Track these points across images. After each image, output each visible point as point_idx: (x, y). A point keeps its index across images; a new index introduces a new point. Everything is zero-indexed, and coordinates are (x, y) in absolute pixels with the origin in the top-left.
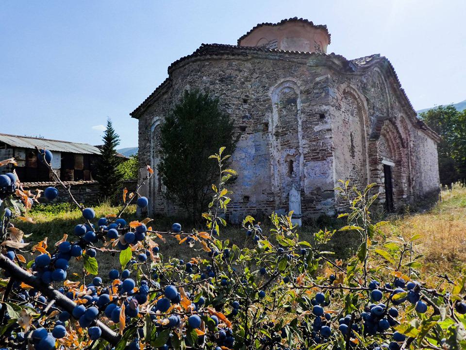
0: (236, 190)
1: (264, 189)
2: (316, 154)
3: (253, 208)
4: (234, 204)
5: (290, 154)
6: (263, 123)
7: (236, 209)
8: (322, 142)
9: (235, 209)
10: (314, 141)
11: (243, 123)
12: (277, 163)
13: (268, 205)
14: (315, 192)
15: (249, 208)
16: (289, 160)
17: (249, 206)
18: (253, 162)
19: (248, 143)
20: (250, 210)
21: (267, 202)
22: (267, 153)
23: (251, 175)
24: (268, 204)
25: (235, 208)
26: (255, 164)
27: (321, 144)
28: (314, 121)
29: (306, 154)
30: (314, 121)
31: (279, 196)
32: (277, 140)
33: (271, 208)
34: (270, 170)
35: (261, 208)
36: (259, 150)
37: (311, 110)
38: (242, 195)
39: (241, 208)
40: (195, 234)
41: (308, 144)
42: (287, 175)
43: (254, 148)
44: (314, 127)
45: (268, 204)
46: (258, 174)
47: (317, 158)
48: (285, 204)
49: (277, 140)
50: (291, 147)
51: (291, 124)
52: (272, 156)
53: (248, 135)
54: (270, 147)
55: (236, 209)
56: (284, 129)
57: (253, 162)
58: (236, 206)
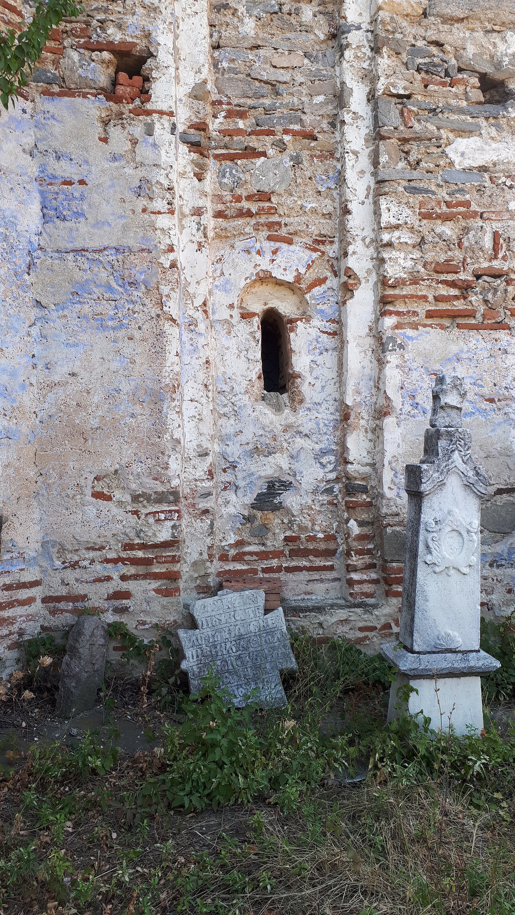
2: (454, 292)
3: (24, 594)
5: (277, 274)
6: (110, 47)
8: (489, 228)
10: (446, 218)
13: (132, 570)
16: (258, 308)
20: (10, 605)
23: (13, 375)
24: (135, 562)
27: (488, 242)
28: (452, 110)
29: (399, 283)
30: (452, 110)
31: (206, 512)
32: (200, 178)
33: (155, 584)
35: (81, 589)
36: (79, 214)
37: (439, 44)
40: (306, 663)
41: (412, 229)
44: (449, 143)
45: (135, 562)
47: (453, 315)
48: (239, 558)
49: (200, 178)
50: (283, 232)
51: (287, 99)
52: (173, 265)
54: (160, 204)
56: (241, 124)
57: (25, 287)
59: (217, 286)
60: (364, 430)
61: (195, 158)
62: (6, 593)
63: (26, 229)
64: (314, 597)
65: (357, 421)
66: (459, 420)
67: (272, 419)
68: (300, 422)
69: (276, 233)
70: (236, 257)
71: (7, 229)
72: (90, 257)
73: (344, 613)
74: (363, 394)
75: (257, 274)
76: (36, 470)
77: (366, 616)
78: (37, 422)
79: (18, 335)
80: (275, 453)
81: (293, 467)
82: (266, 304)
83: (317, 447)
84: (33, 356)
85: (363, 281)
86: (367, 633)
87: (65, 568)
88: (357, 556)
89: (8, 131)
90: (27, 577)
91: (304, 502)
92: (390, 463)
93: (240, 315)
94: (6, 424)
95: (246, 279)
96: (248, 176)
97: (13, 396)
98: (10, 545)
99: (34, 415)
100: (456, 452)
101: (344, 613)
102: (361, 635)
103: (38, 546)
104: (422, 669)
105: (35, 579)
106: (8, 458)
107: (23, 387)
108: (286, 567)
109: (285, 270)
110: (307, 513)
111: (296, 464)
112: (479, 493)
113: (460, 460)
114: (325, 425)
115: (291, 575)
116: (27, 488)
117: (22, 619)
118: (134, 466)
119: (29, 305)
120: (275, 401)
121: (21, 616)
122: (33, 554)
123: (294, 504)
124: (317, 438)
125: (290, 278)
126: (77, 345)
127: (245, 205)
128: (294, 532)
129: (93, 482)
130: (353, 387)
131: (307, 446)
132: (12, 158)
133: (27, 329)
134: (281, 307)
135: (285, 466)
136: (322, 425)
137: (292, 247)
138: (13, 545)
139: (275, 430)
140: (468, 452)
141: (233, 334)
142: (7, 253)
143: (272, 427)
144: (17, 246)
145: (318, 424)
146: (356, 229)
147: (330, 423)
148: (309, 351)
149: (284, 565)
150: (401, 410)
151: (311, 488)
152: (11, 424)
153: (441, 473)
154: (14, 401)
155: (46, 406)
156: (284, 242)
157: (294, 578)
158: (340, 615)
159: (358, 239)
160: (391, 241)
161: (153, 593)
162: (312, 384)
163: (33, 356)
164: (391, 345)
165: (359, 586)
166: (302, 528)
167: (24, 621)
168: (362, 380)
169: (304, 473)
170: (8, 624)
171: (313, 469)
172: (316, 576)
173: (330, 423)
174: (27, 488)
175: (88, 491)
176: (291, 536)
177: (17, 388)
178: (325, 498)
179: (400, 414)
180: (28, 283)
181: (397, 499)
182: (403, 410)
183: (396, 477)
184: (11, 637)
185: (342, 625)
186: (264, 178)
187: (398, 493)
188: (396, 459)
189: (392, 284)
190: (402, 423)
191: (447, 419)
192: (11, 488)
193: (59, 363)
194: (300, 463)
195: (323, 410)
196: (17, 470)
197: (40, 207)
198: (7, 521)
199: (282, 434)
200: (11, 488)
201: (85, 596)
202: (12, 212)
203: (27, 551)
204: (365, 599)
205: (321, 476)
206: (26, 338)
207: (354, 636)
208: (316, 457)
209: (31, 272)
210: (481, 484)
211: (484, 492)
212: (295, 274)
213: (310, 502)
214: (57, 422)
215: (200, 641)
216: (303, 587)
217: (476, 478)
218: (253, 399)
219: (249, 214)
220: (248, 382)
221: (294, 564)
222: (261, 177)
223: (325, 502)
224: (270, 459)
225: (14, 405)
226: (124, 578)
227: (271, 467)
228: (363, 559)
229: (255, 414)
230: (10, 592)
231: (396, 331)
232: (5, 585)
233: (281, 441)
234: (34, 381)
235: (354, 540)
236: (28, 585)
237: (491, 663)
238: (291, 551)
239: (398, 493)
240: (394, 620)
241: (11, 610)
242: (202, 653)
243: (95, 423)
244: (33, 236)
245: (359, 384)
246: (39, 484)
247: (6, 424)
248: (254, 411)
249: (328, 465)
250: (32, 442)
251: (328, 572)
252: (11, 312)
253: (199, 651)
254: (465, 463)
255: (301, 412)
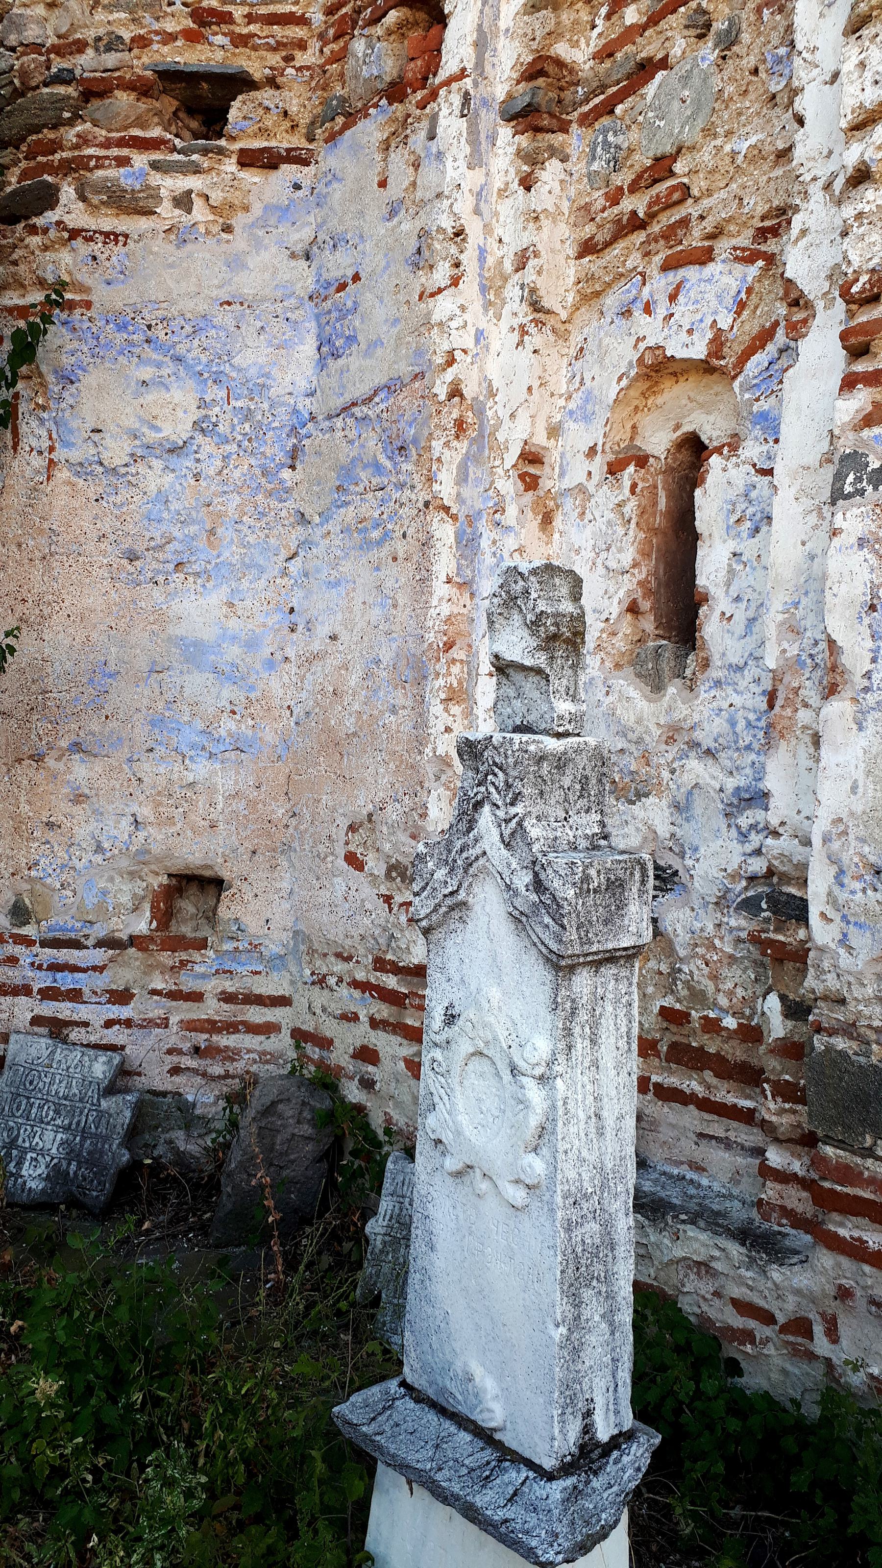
0: (79, 798)
1: (363, 805)
3: (256, 1015)
4: (48, 955)
5: (675, 349)
7: (64, 1010)
9: (48, 1009)
11: (192, 37)
12: (508, 486)
14: (779, 394)
15: (211, 1009)
17: (211, 986)
18: (283, 492)
19: (236, 263)
20: (231, 1027)
21: (380, 964)
22: (405, 369)
23: (251, 644)
25: (49, 994)
26: (302, 519)
32: (527, 183)
34: (424, 581)
38: (143, 857)
39: (122, 997)
42: (620, 644)
43: (312, 325)
46: (323, 630)
50: (694, 239)
52: (455, 392)
53: (251, 177)
54: (442, 274)
55: (64, 1010)
57: (283, 492)
58: (66, 981)
59: (571, 413)
60: (808, 739)
61: (524, 144)
62: (226, 1007)
63: (288, 391)
64: (705, 1182)
65: (788, 712)
66: (545, 707)
67: (642, 712)
68: (696, 717)
69: (680, 248)
70: (606, 334)
71: (252, 399)
72: (359, 415)
73: (704, 1245)
74: (808, 634)
75: (641, 360)
76: (288, 806)
77: (749, 1274)
78: (292, 724)
79: (265, 576)
80: (646, 795)
81: (679, 832)
82: (678, 427)
83: (731, 784)
84: (292, 610)
85: (820, 305)
86: (752, 1324)
87: (313, 983)
88: (779, 1099)
89: (261, 233)
90: (266, 987)
91: (697, 925)
92: (826, 840)
93: (606, 468)
94: (234, 727)
95: (620, 379)
96: (634, 135)
97: (252, 680)
98: (234, 928)
99: (288, 712)
100: (487, 809)
101: (704, 1245)
102: (738, 1322)
103: (286, 936)
104: (366, 1435)
105: (280, 993)
106: (236, 782)
107: (270, 664)
108: (657, 1085)
109: (690, 332)
110: (703, 957)
111: (686, 825)
112: (544, 950)
113: (495, 832)
114: (749, 724)
115: (666, 1109)
116: (269, 835)
117: (252, 1056)
118: (389, 809)
119: (286, 522)
120: (650, 666)
121: (249, 1051)
122: (276, 949)
123: (678, 927)
124: (731, 759)
125: (698, 351)
126: (337, 583)
127: (628, 204)
128: (678, 1000)
129: (347, 835)
130: (780, 617)
131: (709, 780)
132: (267, 276)
133: (281, 564)
134: (707, 428)
135: (663, 830)
136: (741, 725)
137: (711, 269)
138: (239, 929)
139: (647, 739)
140: (513, 810)
141: (589, 516)
142: (250, 440)
143: (640, 729)
144: (270, 423)
145: (733, 723)
146: (811, 164)
147: (759, 719)
148: (728, 528)
149: (655, 1078)
150: (868, 675)
151: (712, 892)
152: (243, 727)
153: (452, 870)
154: (252, 688)
155: (304, 695)
156: (691, 263)
157: (672, 1118)
158: (696, 1246)
159: (816, 191)
160: (864, 162)
161: (402, 1064)
162: (728, 615)
163: (292, 610)
164: (851, 478)
165: (778, 1187)
166: (698, 996)
167: (255, 1061)
168: (806, 593)
169: (702, 850)
170: (225, 1059)
171: (720, 842)
172: (717, 1127)
173: (759, 719)
174: (269, 835)
175: (341, 852)
176: (672, 1009)
177: (258, 666)
178: (743, 923)
179: (866, 690)
180: (289, 484)
181: (842, 951)
182: (875, 676)
183: (842, 885)
184: (229, 1081)
185: (698, 1274)
186: (662, 124)
187: (845, 935)
188: (842, 828)
189: (863, 290)
190: (870, 718)
191: (517, 703)
192: (238, 833)
193: (320, 619)
194: (693, 823)
195: (745, 684)
196: (252, 804)
197: (316, 344)
198: (230, 887)
199: (664, 747)
200: (238, 833)
201: (330, 1042)
202: (261, 367)
203: (267, 942)
204: (788, 1230)
205: (735, 861)
206: (278, 581)
207: (719, 1316)
208: (728, 810)
209: (298, 464)
210: (547, 920)
211: (554, 947)
212: (710, 335)
213: (710, 927)
214: (313, 724)
215: (405, 1188)
216: (688, 1148)
217: (534, 897)
218: (608, 664)
219: (636, 223)
220: (603, 625)
221: (672, 1081)
222: (657, 123)
223: (744, 935)
224: (636, 809)
225: (252, 695)
226: (374, 1024)
227: (637, 829)
228: (795, 1112)
229: (610, 698)
230: (232, 1006)
231: (866, 433)
232: (223, 992)
233: (659, 766)
234: (291, 653)
235: (772, 1051)
236: (268, 1001)
237: (527, 1532)
238: (673, 1046)
239: (845, 935)
240: (823, 1315)
241: (233, 1036)
242: (399, 1215)
243: (350, 724)
244: (302, 398)
245: (796, 605)
246: (291, 830)
247: (234, 727)
248: (608, 693)
249: (753, 833)
250: (284, 759)
251: (742, 1127)
252: (251, 539)
253: (397, 1211)
254: (507, 845)
255: (704, 692)
